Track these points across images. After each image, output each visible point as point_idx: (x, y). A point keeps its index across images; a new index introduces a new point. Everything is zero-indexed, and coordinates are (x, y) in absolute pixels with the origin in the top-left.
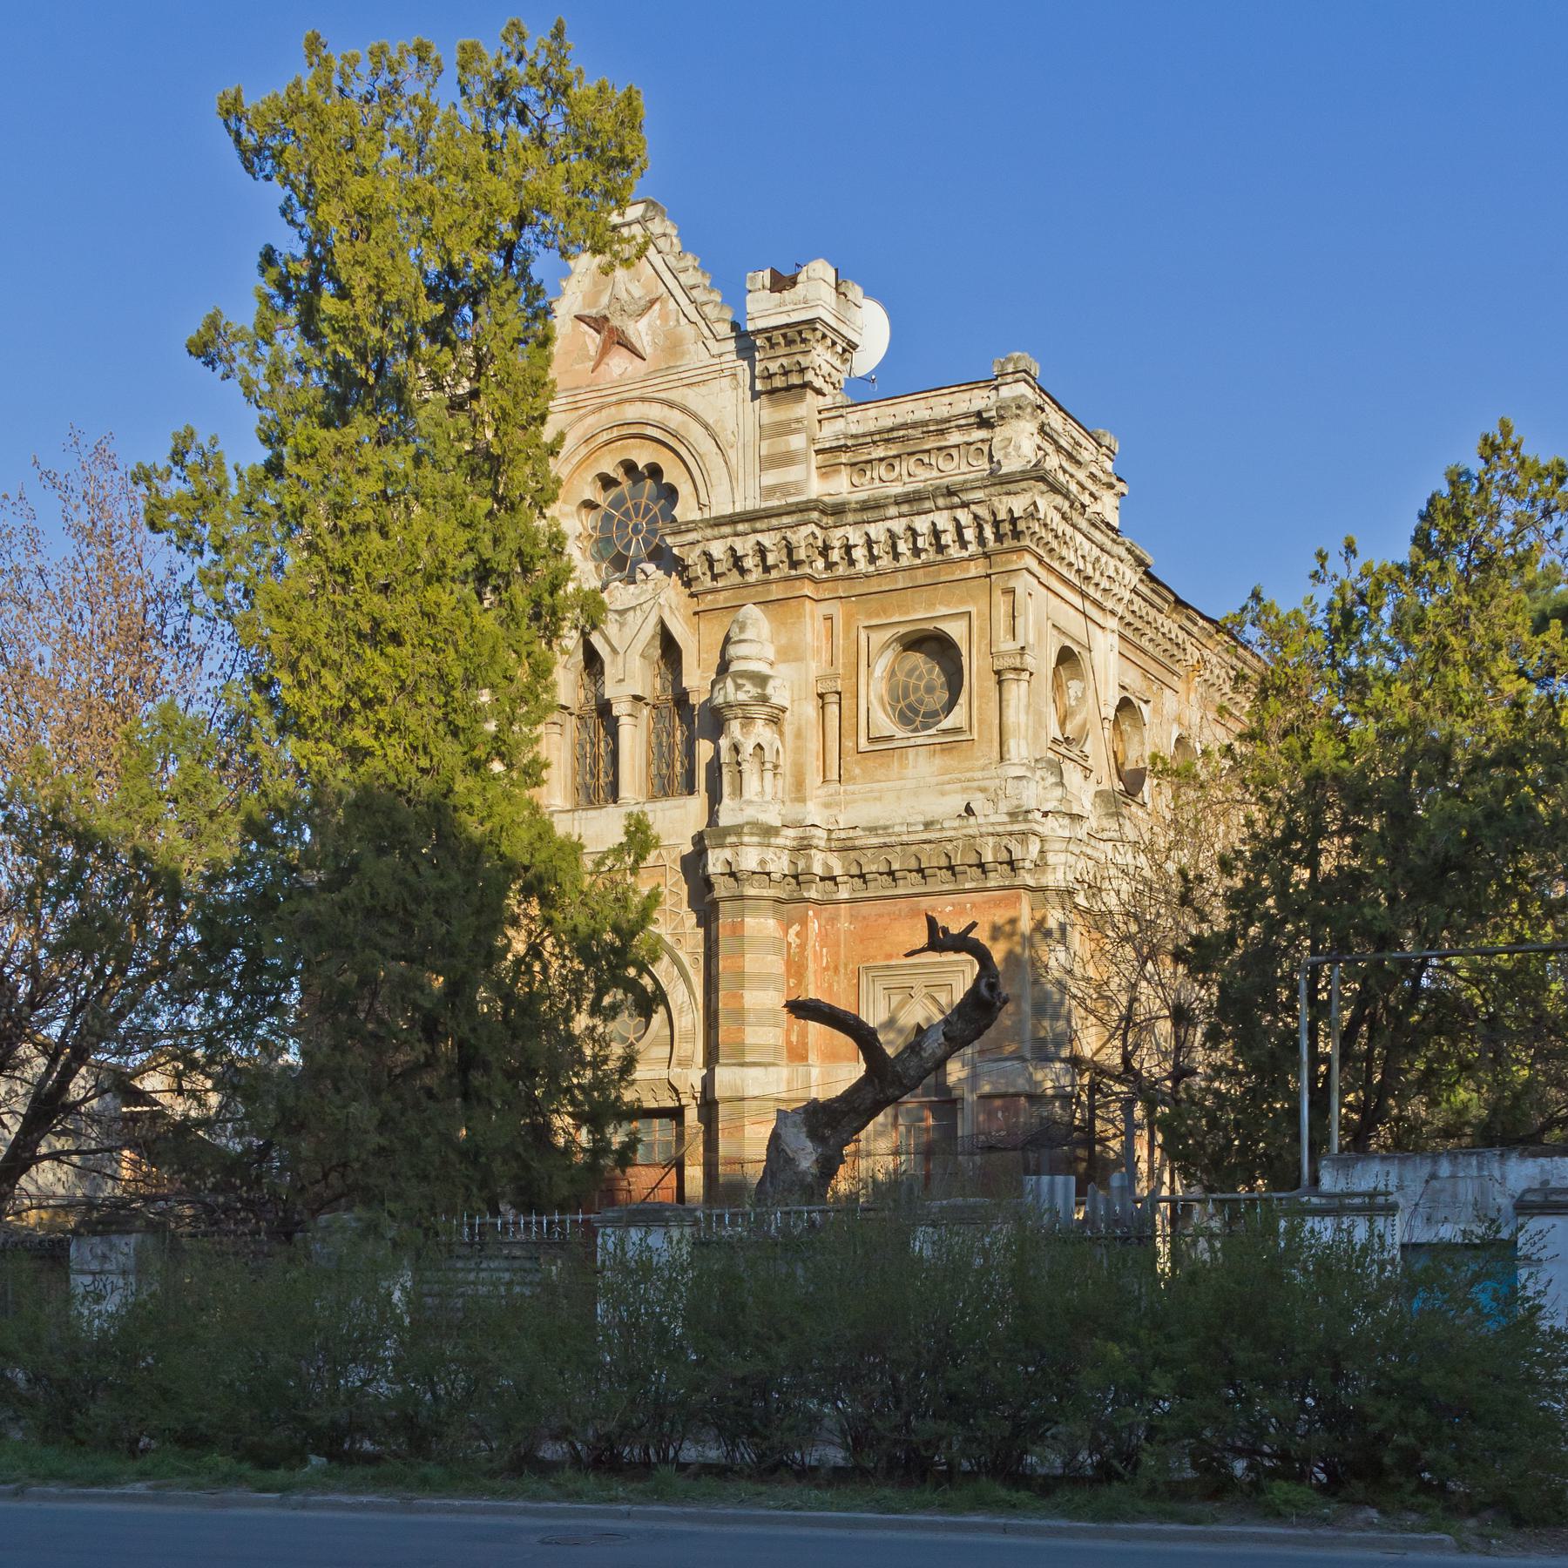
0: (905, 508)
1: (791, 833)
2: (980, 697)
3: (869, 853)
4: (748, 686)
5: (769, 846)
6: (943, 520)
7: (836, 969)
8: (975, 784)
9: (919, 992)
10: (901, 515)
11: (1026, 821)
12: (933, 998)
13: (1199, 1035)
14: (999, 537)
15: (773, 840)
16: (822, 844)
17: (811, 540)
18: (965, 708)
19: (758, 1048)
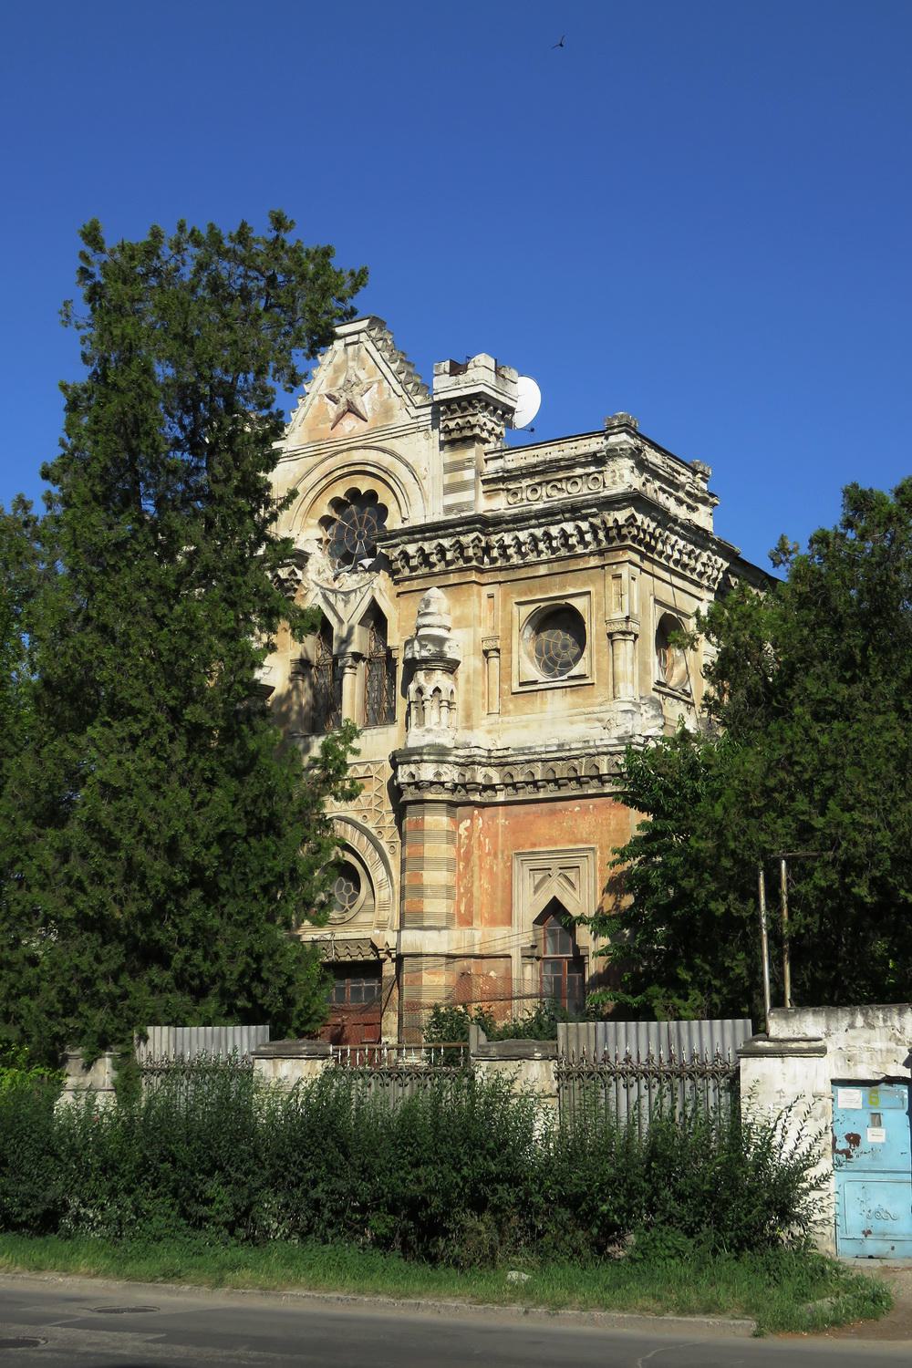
3: (518, 767)
6: (569, 527)
9: (555, 872)
12: (566, 877)
14: (610, 539)
17: (477, 542)
19: (434, 915)
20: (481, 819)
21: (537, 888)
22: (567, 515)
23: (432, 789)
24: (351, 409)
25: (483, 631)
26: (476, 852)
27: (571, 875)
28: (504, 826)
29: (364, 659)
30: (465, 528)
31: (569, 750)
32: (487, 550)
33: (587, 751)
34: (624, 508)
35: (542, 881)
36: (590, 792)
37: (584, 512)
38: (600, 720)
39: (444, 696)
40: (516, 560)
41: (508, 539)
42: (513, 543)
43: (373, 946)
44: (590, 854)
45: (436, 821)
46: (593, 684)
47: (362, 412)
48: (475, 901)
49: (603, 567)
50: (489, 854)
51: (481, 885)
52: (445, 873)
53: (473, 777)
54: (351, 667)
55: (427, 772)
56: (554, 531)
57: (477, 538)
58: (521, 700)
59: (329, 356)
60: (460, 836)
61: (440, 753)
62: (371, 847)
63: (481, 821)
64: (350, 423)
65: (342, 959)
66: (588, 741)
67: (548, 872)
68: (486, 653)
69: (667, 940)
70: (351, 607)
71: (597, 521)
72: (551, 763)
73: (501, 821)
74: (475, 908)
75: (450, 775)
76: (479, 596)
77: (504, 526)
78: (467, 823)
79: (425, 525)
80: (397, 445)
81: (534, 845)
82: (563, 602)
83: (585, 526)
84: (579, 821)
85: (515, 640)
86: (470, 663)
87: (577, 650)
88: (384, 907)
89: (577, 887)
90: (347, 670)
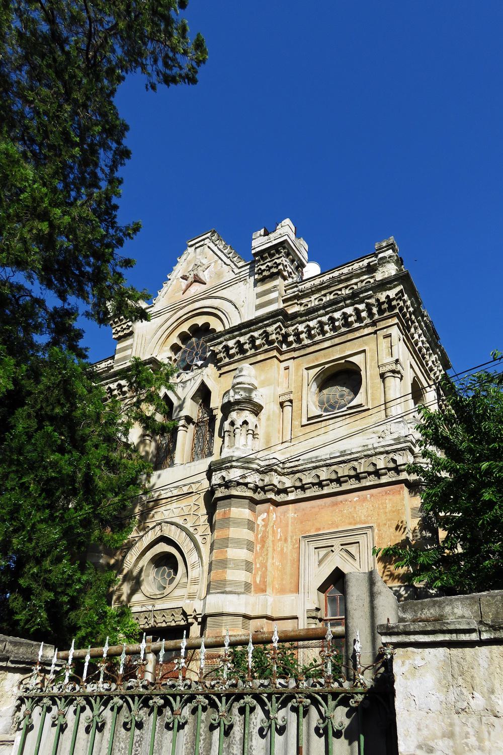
2: (372, 387)
5: (248, 468)
7: (286, 540)
9: (337, 548)
12: (347, 551)
13: (150, 667)
14: (381, 312)
17: (278, 330)
19: (235, 583)
20: (275, 514)
21: (320, 562)
22: (348, 302)
23: (238, 488)
24: (197, 280)
25: (280, 391)
26: (270, 536)
27: (352, 549)
28: (293, 518)
29: (194, 423)
30: (271, 320)
31: (350, 454)
32: (286, 336)
33: (365, 453)
34: (395, 286)
35: (326, 555)
36: (368, 484)
37: (361, 296)
39: (251, 426)
40: (306, 342)
41: (301, 328)
42: (305, 330)
43: (184, 613)
44: (369, 532)
45: (240, 512)
47: (203, 279)
48: (268, 573)
49: (375, 332)
50: (280, 540)
51: (274, 562)
52: (245, 551)
54: (184, 426)
55: (234, 474)
56: (337, 315)
57: (279, 327)
59: (184, 257)
60: (258, 525)
61: (245, 462)
62: (188, 539)
63: (274, 516)
64: (197, 288)
65: (159, 625)
66: (367, 446)
67: (330, 549)
68: (282, 405)
70: (186, 390)
71: (372, 301)
73: (291, 515)
74: (269, 579)
75: (254, 479)
76: (278, 368)
77: (299, 319)
78: (264, 515)
79: (242, 324)
81: (319, 529)
83: (362, 307)
84: (357, 507)
85: (305, 392)
86: (270, 408)
87: (352, 395)
88: (195, 582)
89: (357, 557)
90: (180, 428)
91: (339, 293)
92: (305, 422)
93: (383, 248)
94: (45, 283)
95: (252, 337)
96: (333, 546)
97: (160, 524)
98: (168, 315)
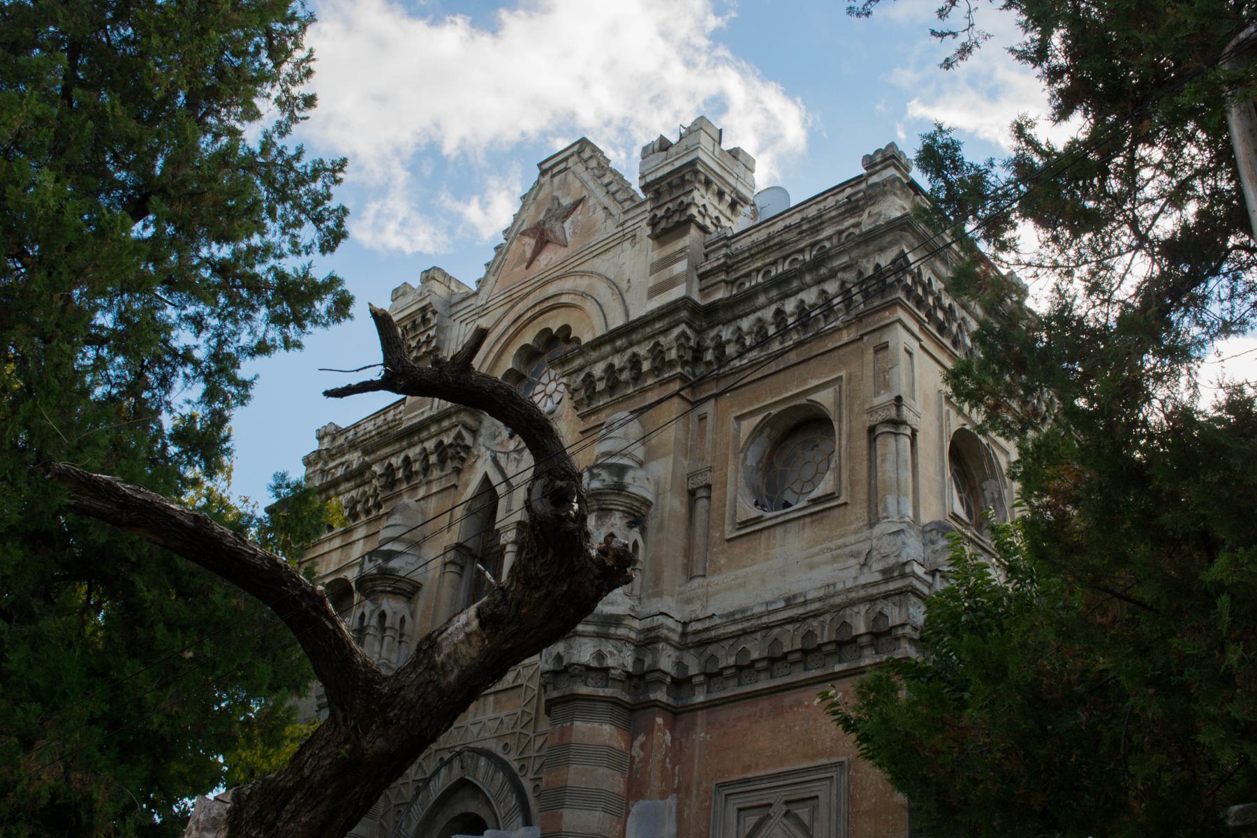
0: (774, 293)
1: (636, 624)
3: (726, 644)
4: (604, 475)
5: (607, 637)
8: (847, 550)
9: (778, 810)
10: (771, 302)
11: (903, 576)
15: (612, 631)
16: (675, 637)
17: (683, 340)
18: (587, 264)
27: (803, 812)
35: (758, 826)
38: (854, 555)
42: (734, 338)
46: (845, 504)
53: (655, 662)
57: (683, 334)
58: (738, 548)
66: (834, 585)
67: (764, 812)
68: (692, 493)
69: (979, 265)
72: (776, 631)
80: (600, 265)
81: (748, 768)
82: (803, 401)
91: (801, 257)
92: (729, 533)
93: (876, 164)
94: (120, 327)
95: (635, 355)
96: (770, 805)
97: (459, 754)
98: (502, 310)
